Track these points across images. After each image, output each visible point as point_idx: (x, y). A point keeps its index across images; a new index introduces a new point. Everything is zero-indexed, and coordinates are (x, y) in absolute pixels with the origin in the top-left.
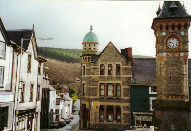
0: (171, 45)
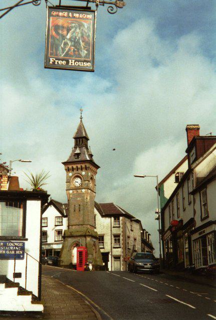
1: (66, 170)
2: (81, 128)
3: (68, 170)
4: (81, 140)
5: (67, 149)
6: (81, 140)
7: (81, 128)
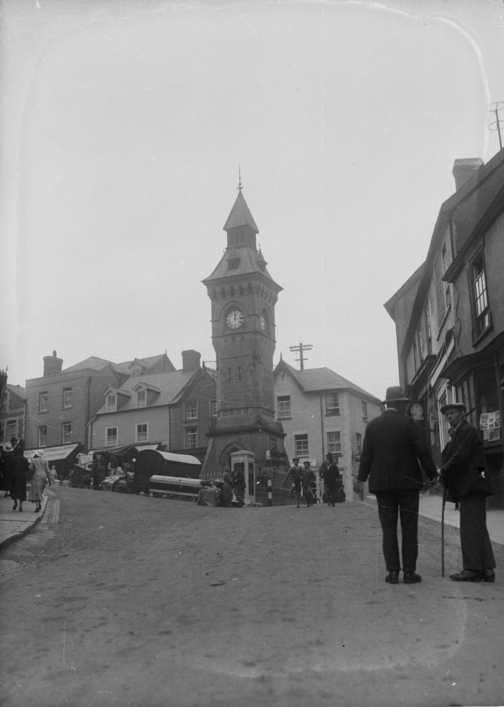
0: (233, 317)
1: (209, 295)
2: (240, 207)
3: (213, 295)
4: (241, 231)
5: (213, 250)
6: (241, 231)
7: (240, 207)
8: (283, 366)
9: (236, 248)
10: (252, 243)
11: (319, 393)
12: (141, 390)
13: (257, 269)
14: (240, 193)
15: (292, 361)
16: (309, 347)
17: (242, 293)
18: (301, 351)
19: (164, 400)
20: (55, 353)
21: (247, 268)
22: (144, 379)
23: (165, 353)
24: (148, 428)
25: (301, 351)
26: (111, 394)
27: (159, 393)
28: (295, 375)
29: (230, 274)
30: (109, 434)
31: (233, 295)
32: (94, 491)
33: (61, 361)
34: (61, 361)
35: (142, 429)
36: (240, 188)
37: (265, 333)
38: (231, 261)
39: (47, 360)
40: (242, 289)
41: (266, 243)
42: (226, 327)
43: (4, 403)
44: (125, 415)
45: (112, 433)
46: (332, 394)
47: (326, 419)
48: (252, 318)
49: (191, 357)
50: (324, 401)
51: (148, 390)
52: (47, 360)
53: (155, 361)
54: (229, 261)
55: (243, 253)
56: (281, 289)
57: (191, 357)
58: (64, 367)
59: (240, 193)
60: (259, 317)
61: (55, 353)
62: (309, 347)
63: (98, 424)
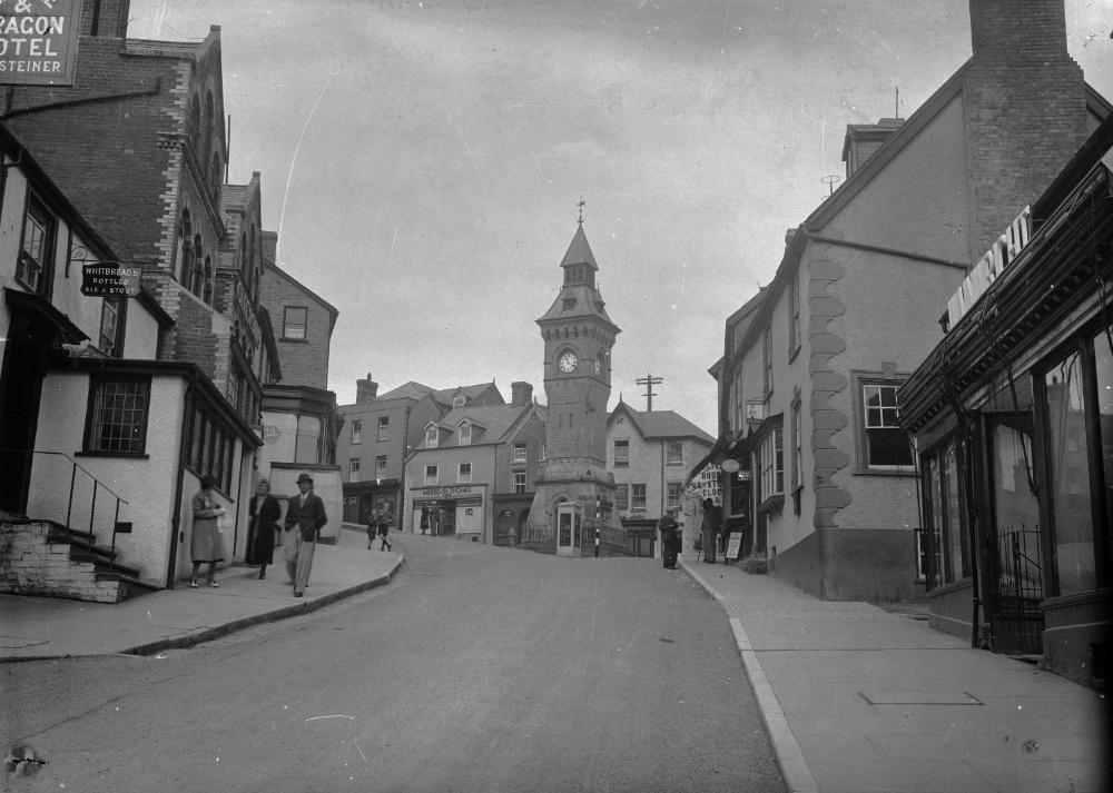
0: (565, 362)
1: (543, 335)
2: (580, 241)
3: (547, 336)
4: (580, 270)
5: (547, 293)
6: (580, 270)
7: (580, 241)
8: (622, 408)
9: (574, 286)
10: (590, 283)
11: (661, 440)
12: (465, 425)
13: (595, 312)
14: (580, 229)
15: (638, 403)
16: (659, 380)
17: (577, 335)
18: (649, 384)
19: (489, 438)
20: (369, 376)
21: (582, 308)
22: (471, 411)
23: (491, 381)
24: (459, 470)
25: (649, 384)
26: (432, 429)
27: (484, 430)
28: (636, 418)
29: (565, 314)
30: (429, 473)
31: (567, 336)
32: (784, 238)
33: (376, 386)
34: (376, 386)
35: (465, 469)
36: (580, 222)
37: (600, 379)
38: (568, 302)
39: (360, 383)
40: (579, 327)
41: (605, 281)
42: (558, 369)
43: (947, 472)
44: (443, 451)
45: (432, 471)
46: (670, 436)
47: (667, 469)
48: (587, 362)
49: (522, 390)
50: (665, 448)
51: (473, 426)
52: (360, 383)
53: (482, 390)
54: (565, 301)
55: (580, 292)
56: (619, 331)
57: (522, 390)
58: (379, 393)
59: (580, 229)
60: (593, 361)
61: (369, 376)
62: (659, 380)
63: (419, 458)
